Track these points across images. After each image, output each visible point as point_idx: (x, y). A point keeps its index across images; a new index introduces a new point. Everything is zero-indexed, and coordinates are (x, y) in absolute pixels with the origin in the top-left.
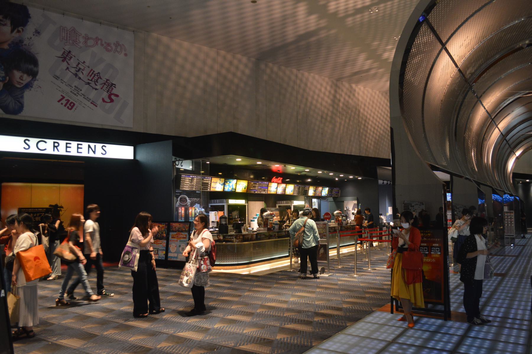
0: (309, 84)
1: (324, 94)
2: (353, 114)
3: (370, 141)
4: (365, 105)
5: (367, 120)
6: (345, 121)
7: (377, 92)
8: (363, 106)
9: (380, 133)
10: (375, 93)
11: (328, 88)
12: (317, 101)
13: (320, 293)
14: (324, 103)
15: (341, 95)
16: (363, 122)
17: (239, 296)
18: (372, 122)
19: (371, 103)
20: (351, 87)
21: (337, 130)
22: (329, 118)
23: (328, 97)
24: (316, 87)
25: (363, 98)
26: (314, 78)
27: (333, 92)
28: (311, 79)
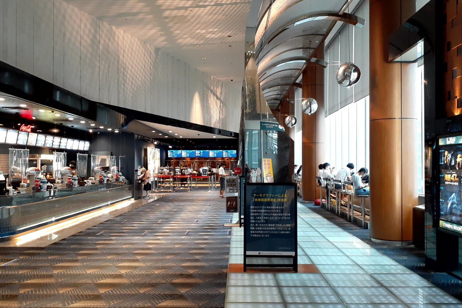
0: (67, 16)
1: (84, 31)
4: (124, 51)
5: (126, 68)
7: (136, 39)
8: (122, 52)
9: (137, 84)
10: (135, 40)
11: (88, 25)
13: (144, 261)
14: (83, 42)
15: (102, 36)
16: (122, 70)
17: (51, 276)
18: (131, 71)
19: (130, 50)
20: (112, 29)
23: (88, 36)
27: (93, 31)
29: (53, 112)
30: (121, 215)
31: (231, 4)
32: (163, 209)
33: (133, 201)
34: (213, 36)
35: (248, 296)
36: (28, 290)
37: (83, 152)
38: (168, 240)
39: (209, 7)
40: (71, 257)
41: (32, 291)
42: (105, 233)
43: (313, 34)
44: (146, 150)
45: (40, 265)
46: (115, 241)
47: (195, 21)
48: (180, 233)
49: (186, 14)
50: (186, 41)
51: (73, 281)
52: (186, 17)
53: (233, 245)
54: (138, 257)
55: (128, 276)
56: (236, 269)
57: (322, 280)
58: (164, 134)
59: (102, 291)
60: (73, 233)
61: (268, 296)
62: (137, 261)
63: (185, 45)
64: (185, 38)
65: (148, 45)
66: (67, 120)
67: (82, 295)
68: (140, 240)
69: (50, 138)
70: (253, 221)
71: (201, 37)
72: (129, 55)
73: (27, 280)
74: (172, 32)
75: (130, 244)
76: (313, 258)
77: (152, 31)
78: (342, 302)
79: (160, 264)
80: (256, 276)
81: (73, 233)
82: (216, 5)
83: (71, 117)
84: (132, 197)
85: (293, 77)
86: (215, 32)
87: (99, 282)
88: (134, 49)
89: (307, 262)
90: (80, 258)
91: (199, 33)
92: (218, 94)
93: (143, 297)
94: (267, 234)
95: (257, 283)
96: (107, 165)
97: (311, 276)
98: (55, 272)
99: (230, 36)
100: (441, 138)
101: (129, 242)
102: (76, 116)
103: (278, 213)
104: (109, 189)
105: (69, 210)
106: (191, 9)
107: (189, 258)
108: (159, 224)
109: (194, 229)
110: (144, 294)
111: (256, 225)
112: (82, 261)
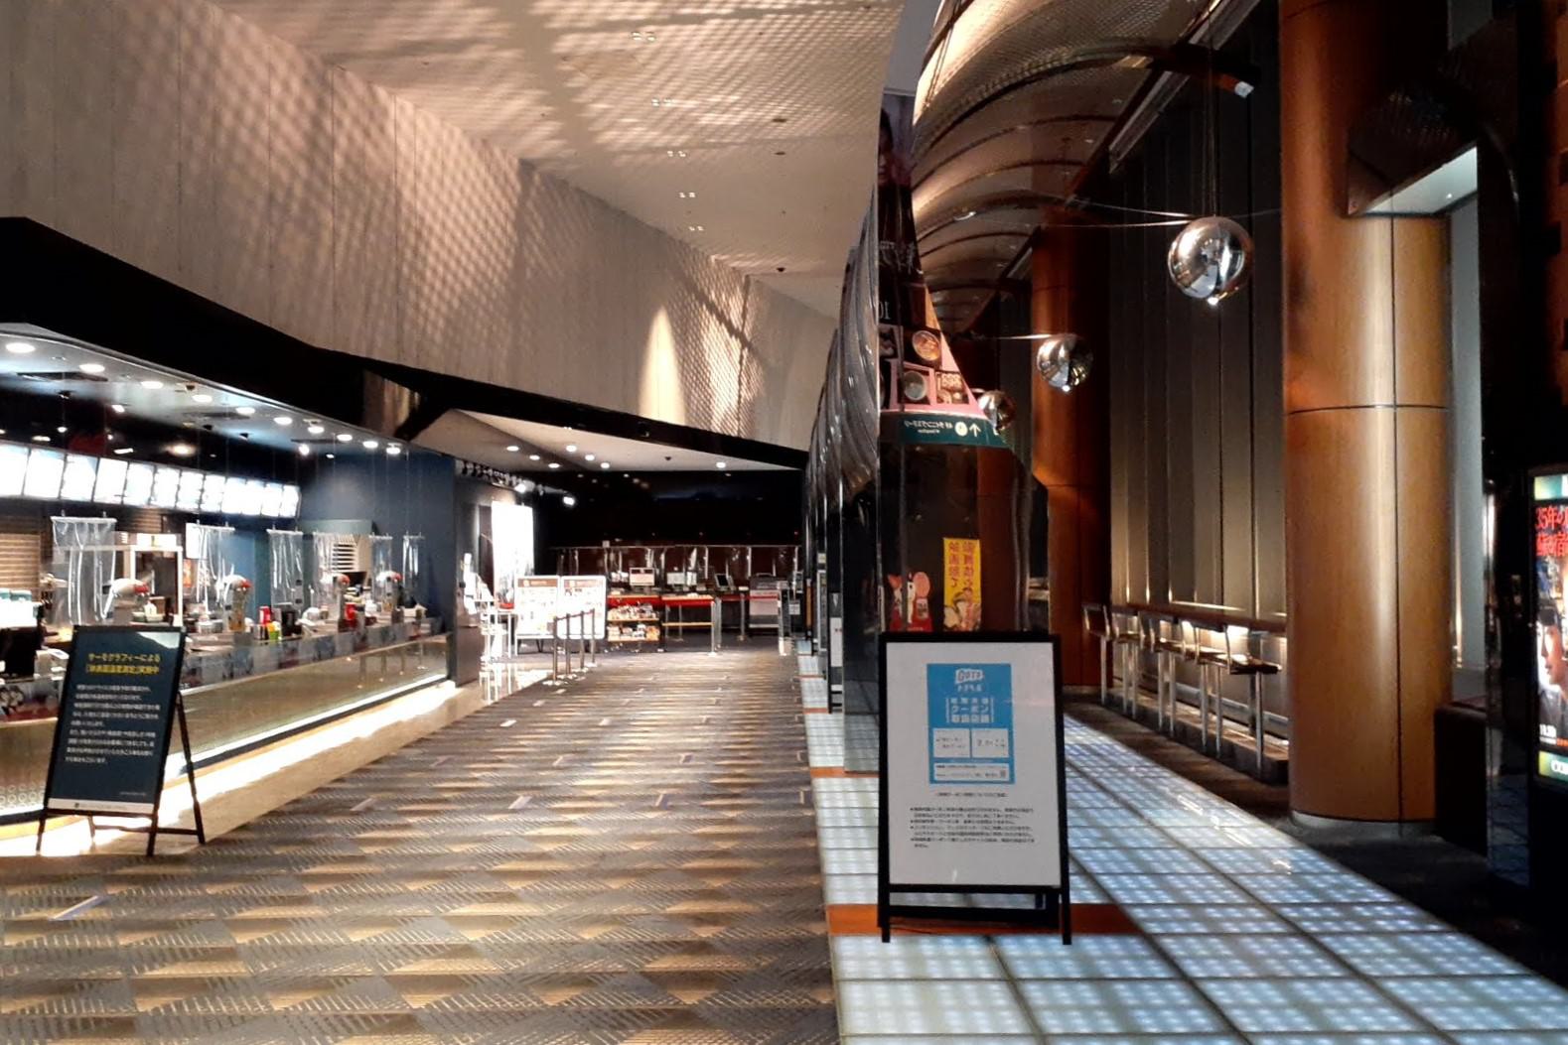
0: (226, 59)
1: (281, 107)
2: (374, 197)
3: (432, 314)
4: (417, 174)
5: (425, 233)
7: (458, 132)
8: (410, 176)
9: (463, 285)
10: (451, 134)
11: (296, 85)
12: (254, 131)
13: (539, 898)
14: (280, 145)
16: (412, 239)
17: (230, 954)
18: (441, 242)
19: (437, 168)
21: (322, 255)
22: (295, 208)
23: (295, 121)
24: (250, 73)
25: (411, 144)
26: (242, 33)
27: (310, 103)
28: (232, 37)
29: (190, 388)
30: (420, 741)
31: (792, 10)
32: (559, 716)
33: (450, 690)
34: (723, 119)
35: (913, 1014)
36: (164, 1000)
37: (284, 523)
38: (603, 824)
39: (713, 23)
40: (283, 887)
41: (179, 1005)
42: (381, 802)
43: (1076, 118)
44: (486, 511)
45: (183, 916)
46: (421, 833)
47: (662, 68)
48: (640, 801)
49: (631, 47)
52: (632, 56)
53: (828, 840)
54: (515, 886)
55: (495, 951)
56: (850, 921)
57: (1151, 957)
58: (548, 455)
59: (417, 1002)
61: (979, 1014)
62: (511, 897)
63: (624, 151)
64: (629, 125)
65: (497, 152)
66: (232, 415)
67: (350, 1017)
68: (507, 825)
69: (168, 475)
70: (78, 723)
71: (684, 121)
72: (434, 184)
73: (152, 968)
74: (582, 107)
76: (1109, 882)
78: (1231, 1029)
80: (927, 946)
81: (273, 807)
82: (740, 14)
83: (243, 402)
84: (449, 678)
85: (1002, 260)
86: (734, 104)
87: (397, 971)
88: (451, 165)
90: (312, 889)
91: (674, 110)
92: (735, 317)
93: (556, 1019)
94: (100, 756)
95: (935, 970)
96: (356, 569)
97: (1113, 944)
98: (242, 939)
99: (782, 121)
100: (1538, 475)
103: (135, 702)
104: (362, 652)
105: (247, 722)
106: (652, 28)
107: (687, 887)
108: (559, 769)
110: (560, 1008)
111: (83, 732)
112: (325, 900)
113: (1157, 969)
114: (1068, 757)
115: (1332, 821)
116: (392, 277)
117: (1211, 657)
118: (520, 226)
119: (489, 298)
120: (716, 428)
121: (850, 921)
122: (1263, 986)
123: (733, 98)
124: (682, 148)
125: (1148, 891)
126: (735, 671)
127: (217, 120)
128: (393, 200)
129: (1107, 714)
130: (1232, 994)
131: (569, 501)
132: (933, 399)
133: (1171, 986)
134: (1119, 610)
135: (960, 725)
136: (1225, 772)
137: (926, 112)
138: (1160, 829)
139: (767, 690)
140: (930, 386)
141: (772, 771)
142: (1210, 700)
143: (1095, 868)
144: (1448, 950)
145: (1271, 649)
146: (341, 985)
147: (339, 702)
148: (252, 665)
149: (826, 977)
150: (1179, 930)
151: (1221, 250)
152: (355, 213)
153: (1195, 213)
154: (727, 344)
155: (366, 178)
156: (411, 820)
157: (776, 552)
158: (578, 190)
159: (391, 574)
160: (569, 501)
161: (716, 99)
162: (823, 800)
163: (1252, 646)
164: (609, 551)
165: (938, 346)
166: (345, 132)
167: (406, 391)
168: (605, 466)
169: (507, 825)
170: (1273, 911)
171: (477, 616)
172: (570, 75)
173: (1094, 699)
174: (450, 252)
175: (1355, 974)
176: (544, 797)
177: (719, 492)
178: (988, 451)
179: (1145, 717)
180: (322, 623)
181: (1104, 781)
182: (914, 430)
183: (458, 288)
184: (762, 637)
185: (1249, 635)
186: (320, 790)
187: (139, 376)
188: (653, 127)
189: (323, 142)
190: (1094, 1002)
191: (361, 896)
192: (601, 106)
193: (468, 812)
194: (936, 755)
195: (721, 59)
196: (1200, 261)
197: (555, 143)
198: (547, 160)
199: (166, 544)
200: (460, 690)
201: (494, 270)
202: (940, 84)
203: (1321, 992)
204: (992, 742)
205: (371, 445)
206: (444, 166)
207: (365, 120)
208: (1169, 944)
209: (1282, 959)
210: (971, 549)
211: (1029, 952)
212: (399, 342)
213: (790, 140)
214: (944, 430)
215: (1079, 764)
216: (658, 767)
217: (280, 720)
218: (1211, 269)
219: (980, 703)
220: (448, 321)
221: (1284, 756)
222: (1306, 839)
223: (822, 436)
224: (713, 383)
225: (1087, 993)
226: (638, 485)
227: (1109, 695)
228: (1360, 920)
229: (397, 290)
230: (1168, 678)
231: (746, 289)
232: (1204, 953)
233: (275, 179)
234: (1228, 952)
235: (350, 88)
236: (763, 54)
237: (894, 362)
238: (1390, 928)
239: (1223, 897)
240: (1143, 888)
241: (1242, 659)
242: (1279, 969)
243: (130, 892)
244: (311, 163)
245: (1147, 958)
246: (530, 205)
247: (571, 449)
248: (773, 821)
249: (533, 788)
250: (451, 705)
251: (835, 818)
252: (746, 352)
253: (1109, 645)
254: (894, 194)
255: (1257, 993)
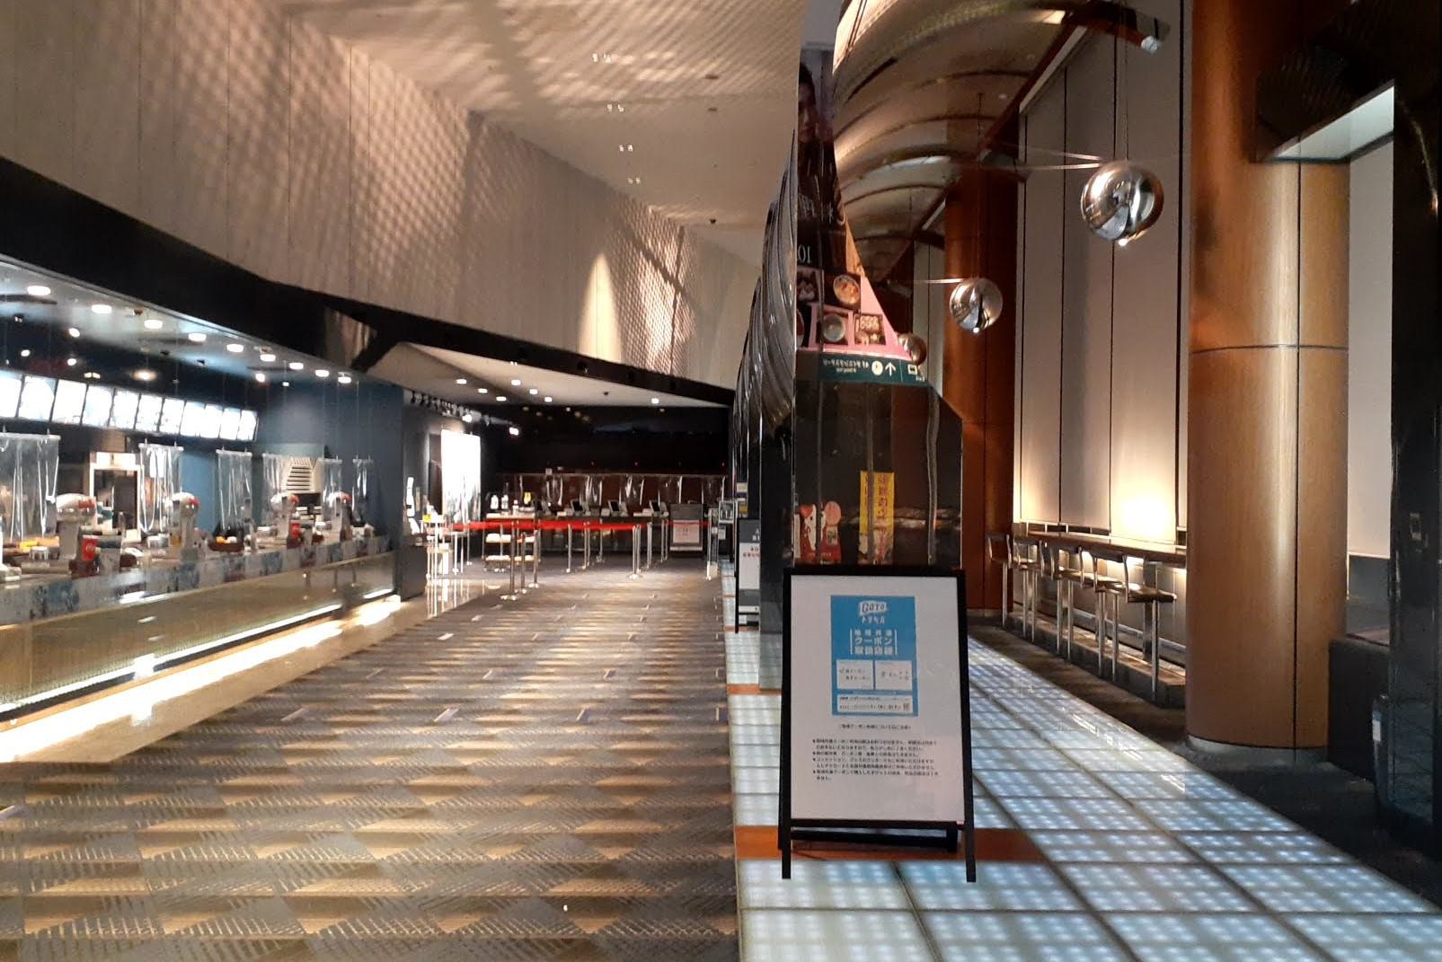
1: (240, 53)
2: (330, 144)
3: (383, 253)
4: (370, 121)
5: (378, 177)
6: (307, 171)
7: (410, 84)
8: (364, 123)
9: (413, 227)
11: (255, 34)
12: (214, 76)
13: (449, 815)
14: (238, 90)
15: (297, 72)
17: (132, 870)
18: (393, 186)
19: (390, 117)
20: (330, 47)
21: (278, 195)
22: (252, 150)
23: (254, 68)
24: (210, 20)
27: (268, 51)
29: (138, 313)
32: (494, 631)
33: (395, 604)
37: (237, 446)
38: (524, 738)
42: (312, 713)
44: (437, 440)
45: (95, 828)
47: (601, 25)
48: (564, 714)
50: (569, 92)
51: (207, 889)
53: (741, 758)
54: (429, 802)
55: (404, 871)
56: (753, 843)
58: (496, 389)
60: (206, 712)
62: (423, 813)
63: (567, 103)
64: (571, 80)
65: (448, 103)
66: (183, 341)
67: (241, 942)
68: (429, 738)
69: (126, 398)
71: (622, 77)
72: (387, 132)
73: (50, 885)
74: (527, 61)
75: (396, 752)
76: (1012, 806)
77: (460, 58)
79: (505, 827)
83: (196, 329)
88: (403, 113)
89: (997, 823)
90: (230, 802)
91: (612, 65)
92: (670, 265)
95: (840, 897)
96: (312, 490)
97: (1018, 872)
98: (149, 854)
101: (399, 745)
102: (212, 328)
107: (599, 805)
108: (487, 682)
109: (601, 701)
112: (240, 813)
113: (1063, 901)
114: (972, 678)
115: (1229, 747)
116: (345, 216)
117: (1109, 585)
118: (468, 172)
119: (437, 239)
120: (651, 366)
121: (753, 843)
122: (1170, 921)
123: (669, 55)
124: (622, 102)
125: (1052, 816)
126: (663, 591)
127: (177, 62)
128: (347, 144)
129: (1008, 636)
130: (1140, 929)
131: (514, 431)
132: (851, 341)
133: (1078, 920)
134: (1019, 539)
135: (864, 657)
136: (1121, 695)
137: (848, 56)
138: (1059, 751)
139: (698, 610)
140: (849, 328)
141: (687, 693)
142: (1106, 626)
143: (999, 790)
144: (1353, 884)
145: (1166, 581)
146: (238, 906)
147: (283, 615)
148: (197, 579)
149: (729, 905)
150: (1084, 858)
151: (1132, 193)
152: (310, 156)
153: (1109, 157)
154: (662, 289)
155: (321, 124)
156: (338, 731)
157: (706, 482)
158: (526, 143)
159: (340, 494)
160: (514, 431)
161: (652, 56)
162: (738, 717)
163: (1148, 576)
164: (550, 479)
165: (857, 291)
166: (303, 81)
167: (360, 325)
168: (548, 400)
169: (429, 738)
170: (1175, 839)
171: (424, 536)
172: (514, 29)
173: (995, 621)
174: (401, 195)
175: (1261, 909)
176: (470, 709)
177: (653, 426)
178: (899, 388)
179: (1043, 640)
180: (272, 539)
181: (1005, 702)
182: (834, 368)
183: (409, 230)
184: (689, 559)
185: (1145, 566)
186: (256, 700)
187: (88, 300)
188: (593, 82)
189: (281, 89)
190: (1000, 937)
191: (286, 809)
192: (543, 60)
193: (394, 724)
194: (840, 686)
195: (656, 17)
196: (1112, 203)
197: (503, 96)
198: (495, 111)
199: (125, 462)
200: (405, 604)
201: (443, 213)
202: (862, 29)
203: (1230, 930)
204: (896, 674)
205: (322, 374)
206: (396, 114)
207: (320, 67)
208: (1074, 872)
209: (1188, 892)
210: (885, 481)
211: (938, 880)
212: (351, 279)
213: (722, 95)
214: (860, 370)
215: (982, 685)
216: (581, 682)
217: (224, 630)
218: (1122, 211)
219: (884, 634)
220: (397, 258)
221: (1182, 681)
222: (1201, 763)
223: (747, 374)
224: (648, 325)
225: (992, 925)
226: (580, 420)
227: (1009, 619)
228: (1262, 850)
229: (350, 225)
230: (1065, 605)
231: (680, 238)
232: (1109, 883)
233: (234, 121)
234: (1132, 883)
235: (308, 37)
236: (696, 13)
237: (815, 307)
238: (1293, 859)
239: (1125, 823)
240: (1046, 812)
241: (1135, 587)
242: (1185, 902)
243: (48, 802)
244: (269, 108)
245: (1053, 888)
246: (478, 153)
247: (516, 383)
248: (691, 737)
249: (460, 701)
250: (396, 616)
251: (750, 736)
252: (679, 298)
253: (1010, 572)
254: (814, 153)
255: (1165, 930)
